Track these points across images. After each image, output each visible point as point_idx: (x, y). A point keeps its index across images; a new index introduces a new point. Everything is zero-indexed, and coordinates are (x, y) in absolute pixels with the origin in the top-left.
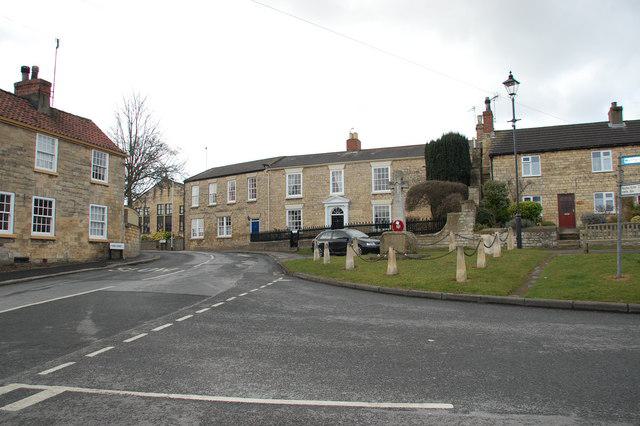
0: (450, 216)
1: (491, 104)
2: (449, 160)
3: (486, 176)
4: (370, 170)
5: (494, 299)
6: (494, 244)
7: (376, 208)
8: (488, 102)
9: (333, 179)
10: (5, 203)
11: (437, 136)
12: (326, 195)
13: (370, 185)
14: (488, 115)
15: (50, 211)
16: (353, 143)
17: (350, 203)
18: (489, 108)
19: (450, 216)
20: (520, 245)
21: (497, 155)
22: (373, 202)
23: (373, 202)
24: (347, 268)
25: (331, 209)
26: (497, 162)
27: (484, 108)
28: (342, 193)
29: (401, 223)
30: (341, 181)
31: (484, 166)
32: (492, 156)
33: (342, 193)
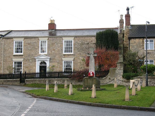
0: (111, 69)
1: (130, 11)
2: (108, 39)
3: (125, 49)
4: (62, 41)
5: (83, 103)
6: (136, 84)
7: (65, 62)
8: (128, 9)
9: (41, 46)
10: (19, 44)
11: (144, 23)
12: (37, 54)
13: (62, 50)
14: (128, 16)
15: (21, 66)
16: (52, 26)
17: (50, 59)
18: (128, 13)
19: (111, 69)
20: (147, 85)
21: (134, 38)
22: (63, 59)
23: (63, 59)
24: (69, 94)
25: (40, 62)
26: (132, 41)
27: (125, 13)
28: (46, 53)
29: (93, 73)
30: (46, 47)
31: (124, 43)
32: (130, 38)
33: (46, 53)
